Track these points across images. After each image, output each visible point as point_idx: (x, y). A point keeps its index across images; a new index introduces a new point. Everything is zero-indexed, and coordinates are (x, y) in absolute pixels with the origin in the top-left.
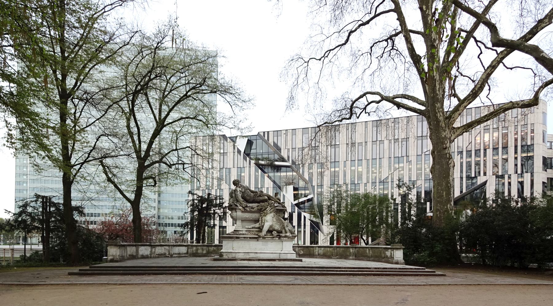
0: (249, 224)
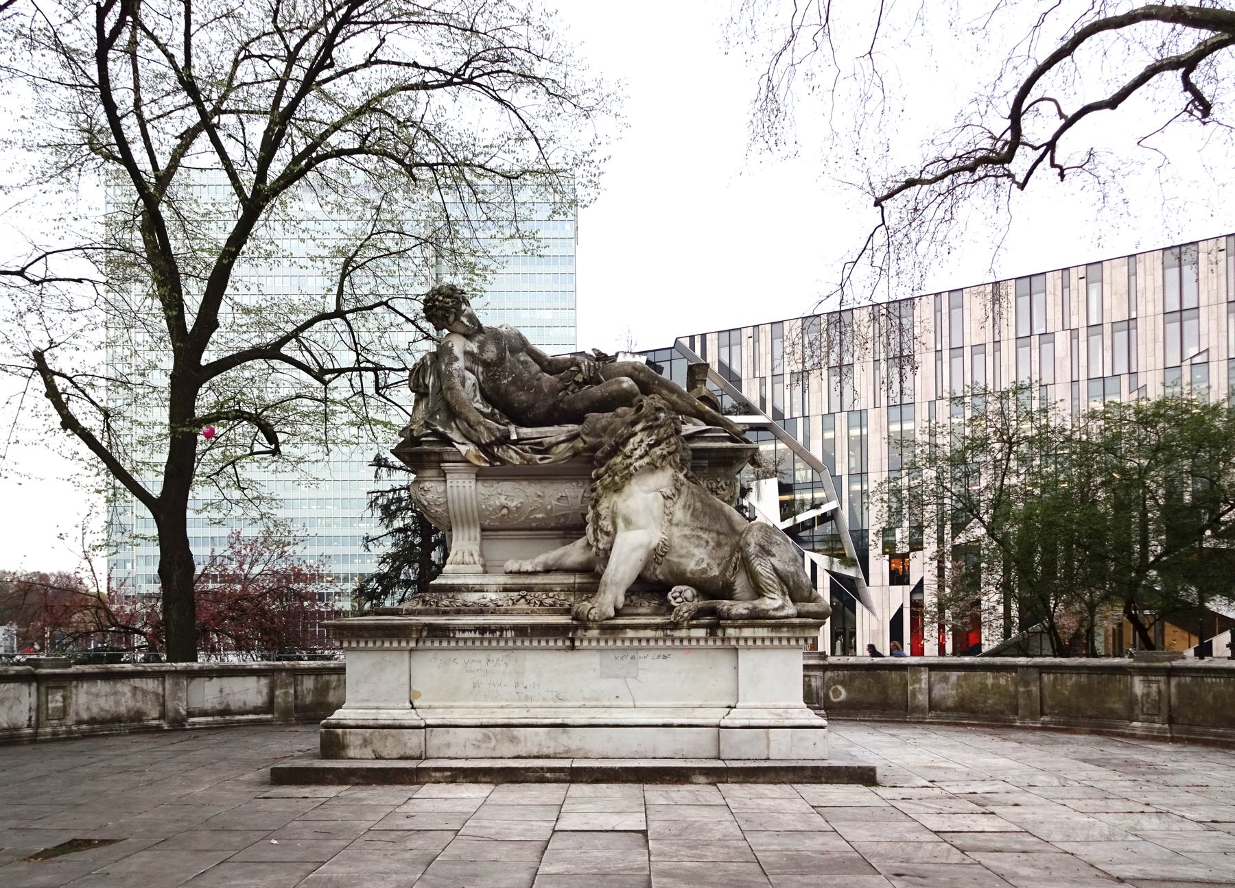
0: (531, 546)
